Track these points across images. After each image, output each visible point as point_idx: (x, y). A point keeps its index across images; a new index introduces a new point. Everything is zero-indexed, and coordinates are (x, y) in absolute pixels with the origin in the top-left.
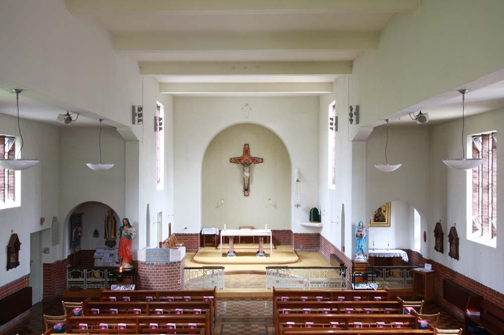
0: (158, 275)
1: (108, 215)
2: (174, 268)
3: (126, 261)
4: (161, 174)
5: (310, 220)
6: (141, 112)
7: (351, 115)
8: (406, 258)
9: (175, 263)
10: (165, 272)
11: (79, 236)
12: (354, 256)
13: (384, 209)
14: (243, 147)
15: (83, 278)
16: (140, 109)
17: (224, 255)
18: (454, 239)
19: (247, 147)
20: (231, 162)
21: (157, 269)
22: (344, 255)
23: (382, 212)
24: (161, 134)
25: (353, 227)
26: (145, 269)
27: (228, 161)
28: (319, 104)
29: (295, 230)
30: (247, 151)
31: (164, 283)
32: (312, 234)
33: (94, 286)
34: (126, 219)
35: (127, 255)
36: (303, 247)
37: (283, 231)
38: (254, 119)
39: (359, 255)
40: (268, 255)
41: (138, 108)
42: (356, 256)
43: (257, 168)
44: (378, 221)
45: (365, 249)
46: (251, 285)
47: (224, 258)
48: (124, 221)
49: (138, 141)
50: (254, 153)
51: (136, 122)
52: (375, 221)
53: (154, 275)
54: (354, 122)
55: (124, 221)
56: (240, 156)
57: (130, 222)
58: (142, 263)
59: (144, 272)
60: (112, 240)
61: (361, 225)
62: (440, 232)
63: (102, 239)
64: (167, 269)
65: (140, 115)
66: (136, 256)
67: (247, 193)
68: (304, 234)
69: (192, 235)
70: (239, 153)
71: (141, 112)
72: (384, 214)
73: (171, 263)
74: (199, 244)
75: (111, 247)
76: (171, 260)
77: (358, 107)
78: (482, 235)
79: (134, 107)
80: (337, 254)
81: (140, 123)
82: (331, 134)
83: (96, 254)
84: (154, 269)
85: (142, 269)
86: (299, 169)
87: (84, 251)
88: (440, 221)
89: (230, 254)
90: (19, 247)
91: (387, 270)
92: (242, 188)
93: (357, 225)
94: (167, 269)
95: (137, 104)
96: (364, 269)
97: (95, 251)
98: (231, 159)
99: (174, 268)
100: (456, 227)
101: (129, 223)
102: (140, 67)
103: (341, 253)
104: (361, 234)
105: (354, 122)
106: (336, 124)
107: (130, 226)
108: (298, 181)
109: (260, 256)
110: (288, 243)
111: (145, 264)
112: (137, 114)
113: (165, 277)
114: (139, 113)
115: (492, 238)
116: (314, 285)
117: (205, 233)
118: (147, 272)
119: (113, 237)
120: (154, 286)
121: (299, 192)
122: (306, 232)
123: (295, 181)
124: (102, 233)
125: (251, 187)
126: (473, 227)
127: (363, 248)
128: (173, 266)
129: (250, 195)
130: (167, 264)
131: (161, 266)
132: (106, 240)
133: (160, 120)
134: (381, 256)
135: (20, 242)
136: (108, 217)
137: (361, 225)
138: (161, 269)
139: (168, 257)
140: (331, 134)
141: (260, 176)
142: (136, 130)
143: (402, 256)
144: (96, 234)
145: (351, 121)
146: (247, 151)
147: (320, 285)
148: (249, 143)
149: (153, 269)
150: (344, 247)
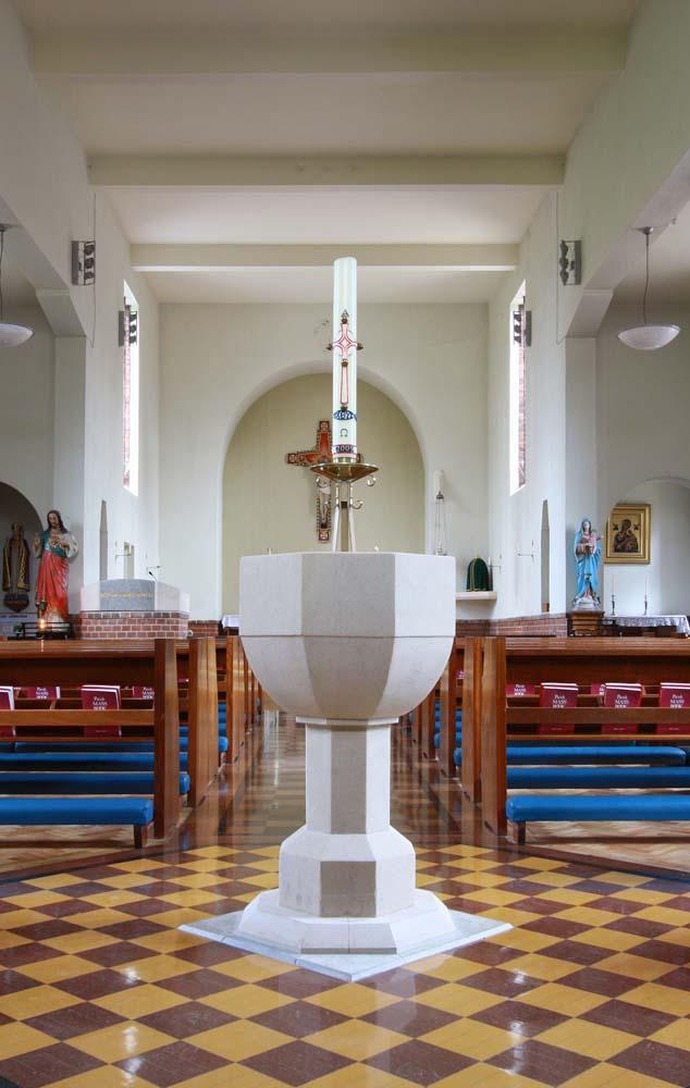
1: (10, 535)
2: (164, 628)
3: (55, 610)
4: (133, 465)
5: (468, 588)
6: (92, 256)
7: (564, 262)
9: (166, 615)
12: (571, 601)
13: (636, 523)
16: (90, 249)
19: (324, 425)
20: (289, 462)
21: (126, 628)
23: (632, 529)
24: (133, 352)
25: (569, 535)
27: (282, 459)
35: (55, 595)
39: (582, 596)
41: (86, 247)
42: (575, 600)
43: (357, 490)
44: (623, 550)
45: (596, 584)
48: (51, 515)
49: (85, 336)
52: (616, 550)
54: (571, 278)
55: (51, 515)
57: (62, 519)
58: (90, 617)
60: (20, 592)
61: (588, 527)
64: (148, 628)
65: (90, 263)
66: (79, 603)
70: (309, 443)
71: (92, 256)
72: (636, 533)
73: (158, 615)
75: (19, 611)
76: (156, 608)
77: (578, 245)
79: (75, 245)
81: (88, 281)
82: (515, 350)
84: (118, 628)
85: (92, 629)
86: (442, 471)
92: (313, 523)
93: (578, 528)
94: (148, 628)
95: (83, 236)
96: (595, 623)
98: (289, 455)
99: (164, 628)
101: (61, 522)
102: (90, 167)
104: (588, 548)
105: (571, 278)
106: (528, 333)
107: (63, 530)
108: (440, 497)
111: (98, 617)
112: (83, 261)
114: (88, 257)
119: (21, 585)
121: (442, 523)
127: (591, 579)
128: (162, 622)
130: (148, 616)
131: (134, 622)
133: (131, 320)
134: (629, 625)
136: (12, 541)
137: (588, 527)
138: (134, 629)
140: (515, 350)
142: (80, 296)
143: (677, 624)
145: (565, 276)
149: (116, 629)
150: (548, 605)
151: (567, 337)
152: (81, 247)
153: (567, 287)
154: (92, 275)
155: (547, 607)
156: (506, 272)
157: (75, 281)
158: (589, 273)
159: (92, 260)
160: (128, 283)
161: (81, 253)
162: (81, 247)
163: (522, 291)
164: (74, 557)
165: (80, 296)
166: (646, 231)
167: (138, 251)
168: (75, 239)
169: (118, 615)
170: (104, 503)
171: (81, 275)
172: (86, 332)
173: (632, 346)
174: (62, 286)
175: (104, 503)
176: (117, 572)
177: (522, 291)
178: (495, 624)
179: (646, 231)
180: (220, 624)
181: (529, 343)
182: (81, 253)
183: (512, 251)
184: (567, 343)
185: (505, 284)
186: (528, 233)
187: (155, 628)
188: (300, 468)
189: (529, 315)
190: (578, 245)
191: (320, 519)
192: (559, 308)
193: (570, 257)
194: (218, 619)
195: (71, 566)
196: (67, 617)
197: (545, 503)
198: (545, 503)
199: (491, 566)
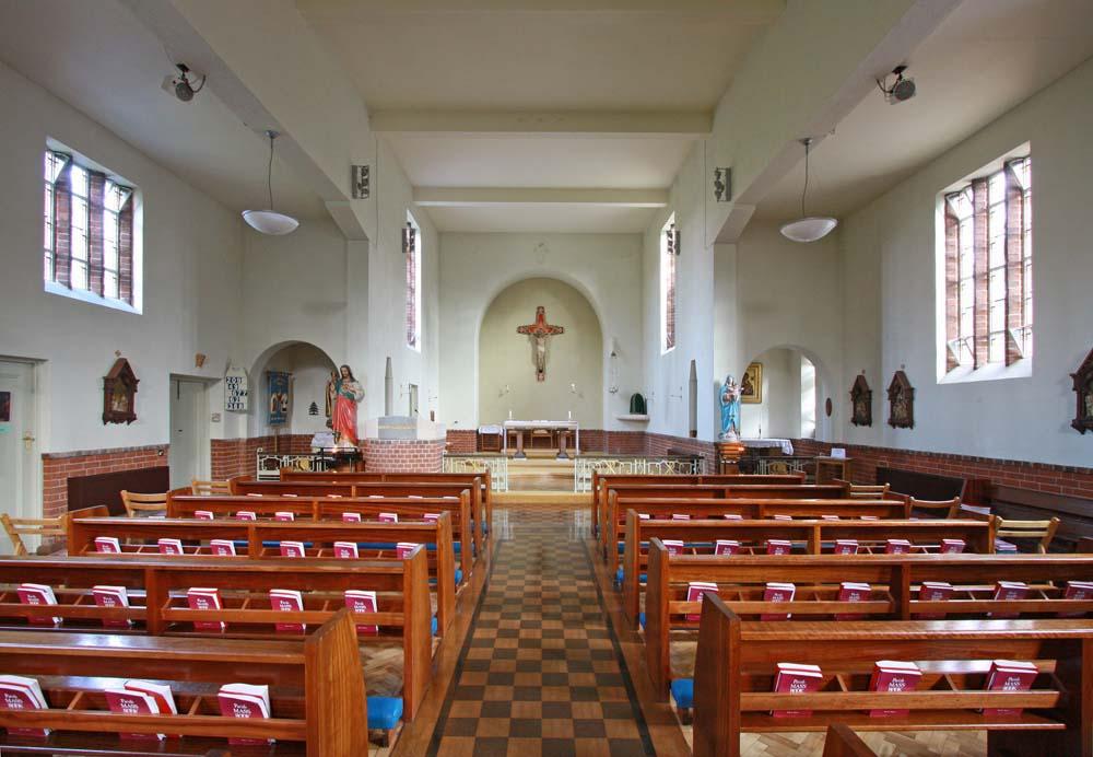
2: (425, 451)
7: (718, 184)
8: (788, 449)
9: (426, 442)
11: (284, 410)
14: (559, 325)
16: (365, 171)
18: (901, 391)
26: (378, 451)
29: (607, 428)
30: (541, 317)
32: (634, 433)
34: (348, 368)
38: (550, 266)
50: (550, 320)
51: (359, 195)
55: (344, 369)
58: (372, 442)
59: (375, 456)
62: (864, 389)
63: (322, 418)
65: (366, 182)
69: (464, 432)
70: (530, 319)
71: (366, 177)
72: (752, 383)
73: (419, 442)
77: (729, 172)
78: (975, 368)
79: (354, 169)
80: (678, 447)
81: (365, 195)
82: (666, 259)
83: (314, 441)
87: (295, 436)
88: (864, 372)
90: (136, 387)
91: (768, 462)
92: (534, 369)
95: (360, 163)
97: (312, 436)
99: (425, 451)
100: (905, 371)
102: (370, 117)
104: (732, 396)
107: (353, 380)
108: (614, 355)
111: (377, 443)
115: (1007, 365)
118: (381, 456)
122: (620, 430)
124: (321, 407)
125: (548, 369)
126: (948, 361)
127: (735, 419)
128: (422, 447)
130: (412, 443)
132: (327, 419)
135: (137, 378)
141: (559, 350)
142: (360, 208)
144: (314, 409)
145: (718, 194)
146: (541, 317)
148: (539, 384)
151: (716, 243)
152: (359, 170)
153: (721, 203)
154: (367, 192)
155: (694, 433)
157: (354, 196)
158: (738, 192)
159: (367, 180)
161: (359, 175)
162: (359, 170)
163: (672, 220)
164: (362, 398)
165: (360, 208)
166: (806, 142)
167: (417, 191)
169: (390, 443)
170: (388, 359)
171: (359, 192)
172: (368, 236)
173: (791, 237)
174: (346, 200)
176: (229, 490)
177: (672, 220)
178: (648, 435)
179: (806, 142)
180: (477, 432)
181: (678, 252)
182: (359, 175)
183: (664, 193)
185: (657, 218)
186: (676, 179)
187: (418, 451)
188: (526, 336)
189: (678, 234)
190: (729, 172)
191: (538, 367)
192: (708, 221)
193: (723, 179)
195: (359, 405)
196: (356, 442)
197: (693, 362)
198: (693, 362)
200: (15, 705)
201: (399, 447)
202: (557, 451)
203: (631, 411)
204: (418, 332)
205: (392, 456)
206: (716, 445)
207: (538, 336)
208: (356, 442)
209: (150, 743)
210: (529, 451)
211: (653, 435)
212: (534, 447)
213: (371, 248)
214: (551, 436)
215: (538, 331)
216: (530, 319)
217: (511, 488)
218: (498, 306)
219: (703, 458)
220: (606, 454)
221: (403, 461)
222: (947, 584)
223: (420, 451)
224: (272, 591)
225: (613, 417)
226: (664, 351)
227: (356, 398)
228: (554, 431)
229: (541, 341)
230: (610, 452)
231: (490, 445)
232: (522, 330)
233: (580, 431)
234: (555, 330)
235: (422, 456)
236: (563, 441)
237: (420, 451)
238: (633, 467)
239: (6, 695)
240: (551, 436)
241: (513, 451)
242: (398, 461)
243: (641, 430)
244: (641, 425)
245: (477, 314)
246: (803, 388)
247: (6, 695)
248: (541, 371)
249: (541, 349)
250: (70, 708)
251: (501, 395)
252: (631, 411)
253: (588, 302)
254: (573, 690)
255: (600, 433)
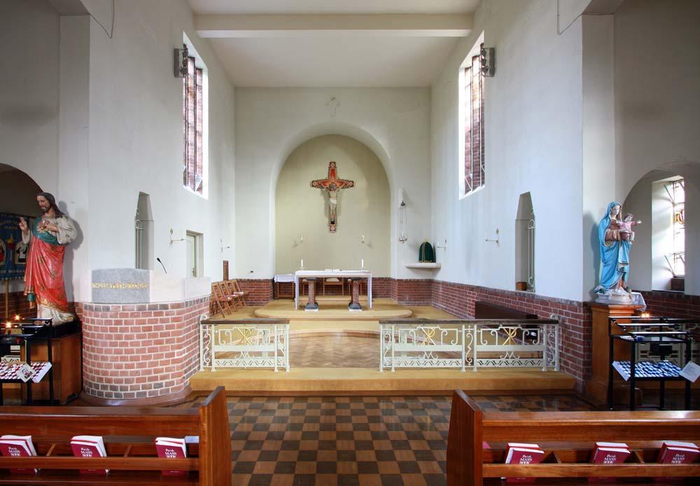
0: (119, 337)
2: (163, 321)
3: (46, 301)
9: (165, 307)
10: (137, 330)
11: (22, 260)
14: (328, 166)
15: (460, 343)
17: (302, 307)
20: (313, 186)
22: (532, 298)
28: (430, 98)
30: (332, 172)
31: (137, 359)
33: (238, 363)
36: (409, 298)
37: (379, 279)
40: (365, 308)
46: (345, 360)
47: (302, 312)
49: (89, 14)
50: (342, 174)
53: (110, 337)
56: (324, 178)
67: (333, 228)
68: (410, 281)
69: (259, 281)
70: (323, 174)
73: (153, 307)
74: (501, 465)
84: (110, 322)
86: (404, 189)
89: (309, 306)
92: (327, 220)
99: (163, 321)
103: (522, 297)
104: (622, 234)
107: (59, 214)
108: (403, 204)
109: (354, 308)
110: (387, 295)
111: (91, 308)
113: (137, 344)
116: (484, 361)
117: (279, 281)
120: (109, 366)
123: (399, 206)
125: (339, 220)
128: (161, 314)
129: (338, 230)
130: (141, 308)
131: (126, 315)
138: (126, 323)
139: (145, 291)
141: (353, 202)
146: (332, 172)
147: (497, 361)
155: (524, 286)
156: (459, 38)
160: (186, 33)
168: (176, 48)
169: (108, 309)
170: (143, 198)
172: (89, 9)
175: (143, 198)
178: (438, 283)
180: (273, 280)
184: (583, 19)
187: (151, 322)
188: (319, 190)
191: (330, 218)
194: (270, 278)
197: (526, 199)
198: (526, 199)
199: (434, 247)
200: (16, 454)
201: (123, 315)
202: (348, 299)
203: (420, 259)
204: (205, 176)
205: (112, 330)
206: (587, 306)
207: (330, 189)
208: (71, 307)
209: (101, 475)
210: (321, 300)
211: (444, 284)
212: (327, 294)
213: (95, 29)
214: (342, 283)
215: (330, 185)
216: (323, 174)
217: (295, 362)
218: (294, 160)
219: (556, 322)
220: (396, 302)
221: (127, 337)
222: (338, 270)
223: (156, 321)
224: (75, 438)
225: (402, 265)
226: (462, 195)
227: (62, 240)
228: (346, 279)
229: (333, 194)
230: (399, 300)
231: (286, 293)
232: (315, 184)
233: (374, 279)
234: (347, 184)
235: (157, 328)
236: (355, 290)
237: (156, 321)
238: (460, 334)
239: (10, 448)
240: (342, 283)
241: (305, 299)
242: (119, 337)
243: (431, 278)
244: (431, 273)
245: (272, 168)
246: (653, 231)
247: (10, 448)
248: (333, 223)
249: (333, 201)
250: (48, 454)
251: (296, 245)
252: (420, 259)
253: (375, 155)
254: (352, 438)
255: (388, 281)
